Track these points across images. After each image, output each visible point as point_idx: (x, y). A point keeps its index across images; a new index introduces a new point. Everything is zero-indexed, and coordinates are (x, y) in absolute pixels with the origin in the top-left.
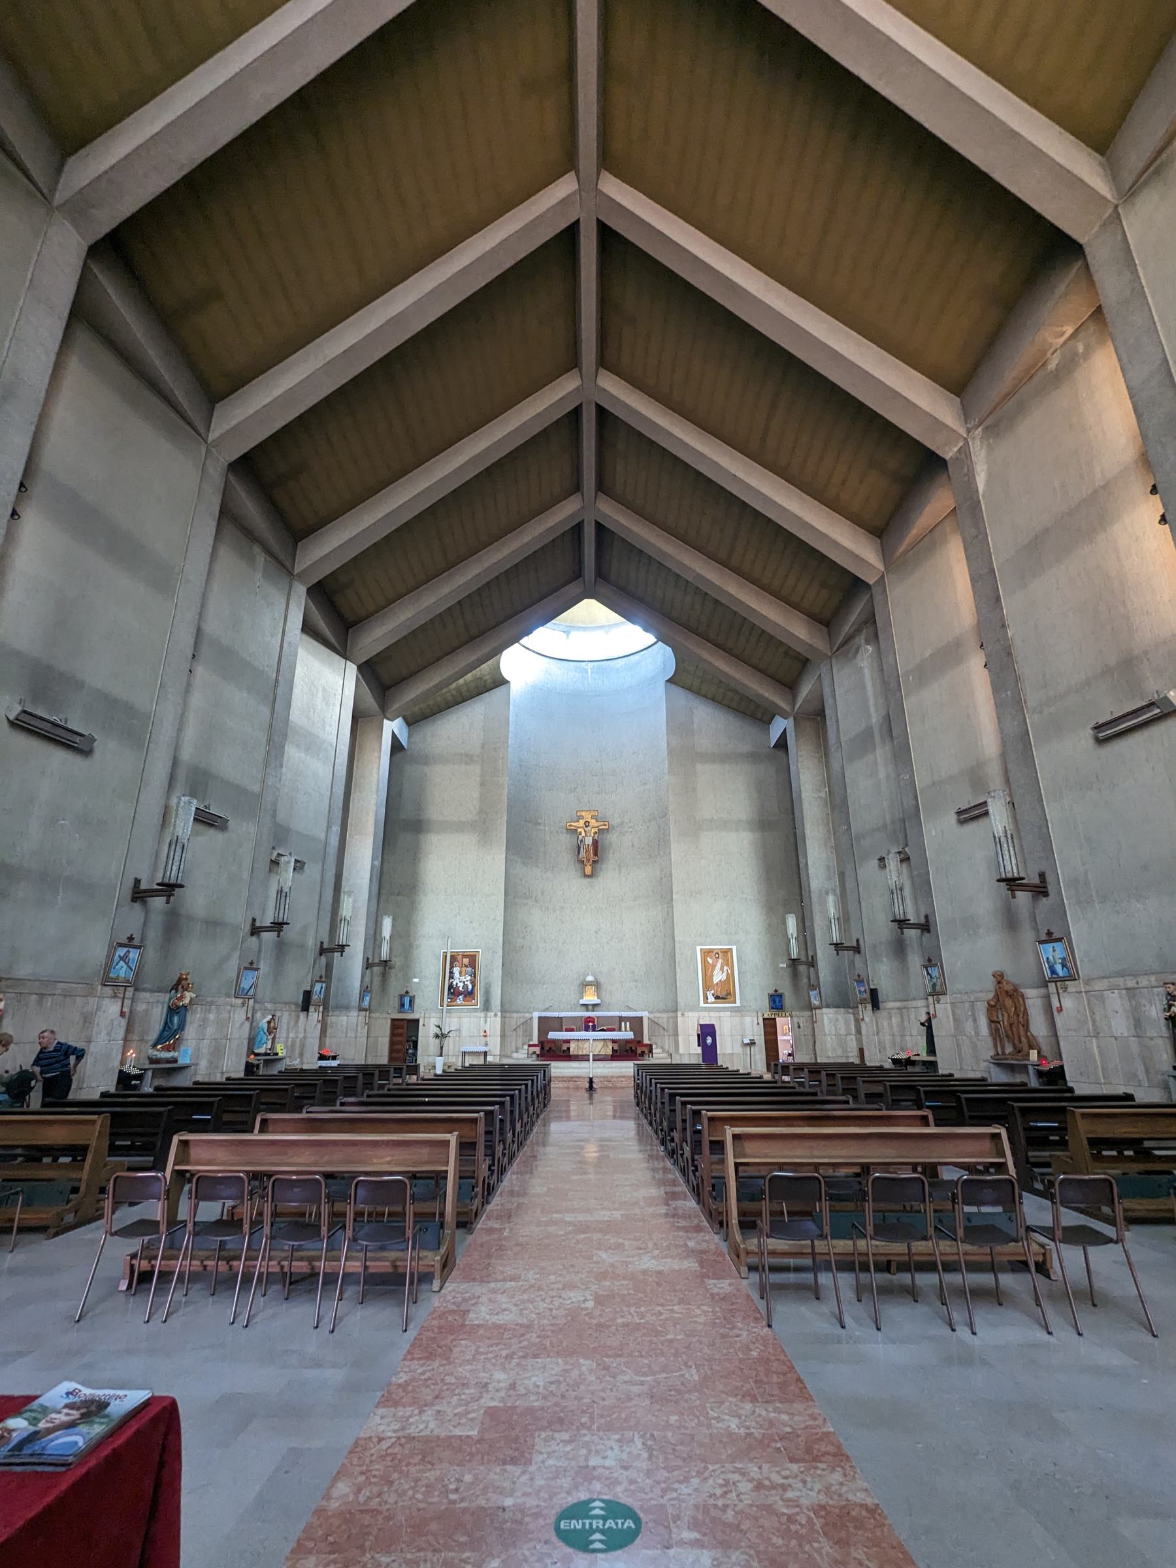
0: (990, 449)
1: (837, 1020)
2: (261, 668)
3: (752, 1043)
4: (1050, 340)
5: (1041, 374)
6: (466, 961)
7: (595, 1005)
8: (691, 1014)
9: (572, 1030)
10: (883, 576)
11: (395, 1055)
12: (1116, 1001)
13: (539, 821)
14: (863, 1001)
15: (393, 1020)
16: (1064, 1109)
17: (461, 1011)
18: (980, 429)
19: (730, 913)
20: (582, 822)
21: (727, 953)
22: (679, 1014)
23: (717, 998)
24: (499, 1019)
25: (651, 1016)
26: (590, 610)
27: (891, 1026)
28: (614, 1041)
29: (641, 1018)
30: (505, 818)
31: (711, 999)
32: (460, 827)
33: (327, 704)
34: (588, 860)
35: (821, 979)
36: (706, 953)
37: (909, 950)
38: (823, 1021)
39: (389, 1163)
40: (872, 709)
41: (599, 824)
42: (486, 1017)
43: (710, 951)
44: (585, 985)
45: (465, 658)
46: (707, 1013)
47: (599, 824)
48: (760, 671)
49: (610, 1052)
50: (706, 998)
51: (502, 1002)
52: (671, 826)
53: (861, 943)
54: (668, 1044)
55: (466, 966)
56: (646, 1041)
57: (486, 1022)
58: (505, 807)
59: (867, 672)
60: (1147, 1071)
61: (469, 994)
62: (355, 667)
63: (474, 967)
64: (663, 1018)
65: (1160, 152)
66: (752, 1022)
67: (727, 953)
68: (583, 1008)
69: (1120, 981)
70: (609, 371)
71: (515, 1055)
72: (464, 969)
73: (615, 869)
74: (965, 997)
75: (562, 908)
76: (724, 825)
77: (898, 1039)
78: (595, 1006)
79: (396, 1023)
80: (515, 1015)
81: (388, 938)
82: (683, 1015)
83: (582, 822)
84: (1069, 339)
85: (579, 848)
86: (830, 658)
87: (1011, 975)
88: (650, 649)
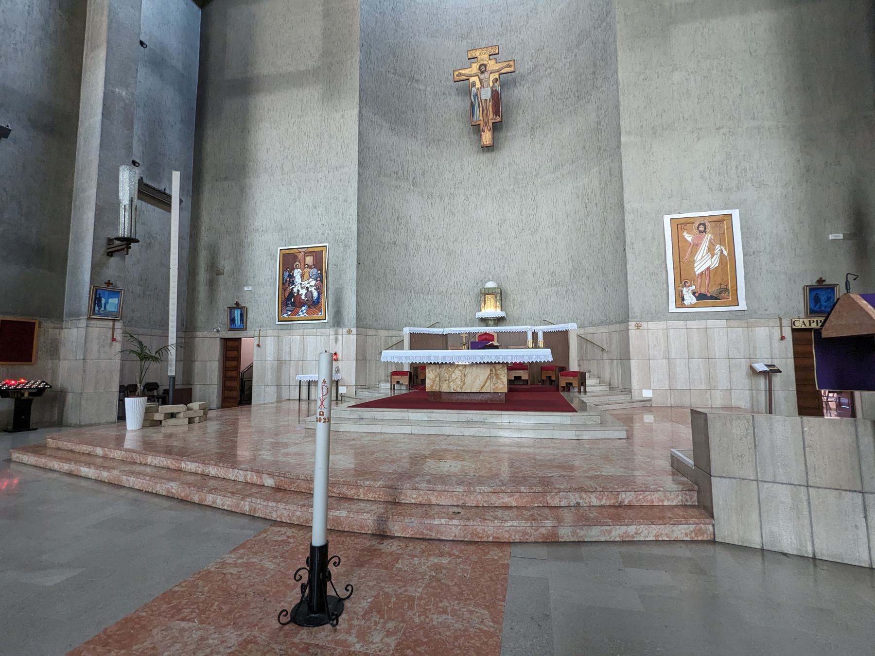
3: (771, 372)
6: (309, 260)
8: (652, 325)
11: (228, 383)
13: (417, 77)
17: (305, 327)
19: (728, 156)
20: (475, 67)
22: (632, 325)
23: (701, 297)
24: (353, 337)
25: (581, 332)
28: (512, 367)
29: (567, 332)
31: (690, 299)
32: (297, 79)
36: (679, 226)
41: (499, 66)
42: (336, 334)
44: (485, 293)
46: (681, 323)
49: (502, 386)
51: (358, 313)
54: (610, 370)
55: (310, 267)
56: (574, 367)
57: (336, 340)
61: (314, 304)
63: (320, 269)
64: (601, 334)
66: (771, 338)
72: (307, 270)
75: (453, 195)
78: (499, 321)
79: (229, 343)
80: (383, 333)
82: (638, 327)
85: (473, 106)
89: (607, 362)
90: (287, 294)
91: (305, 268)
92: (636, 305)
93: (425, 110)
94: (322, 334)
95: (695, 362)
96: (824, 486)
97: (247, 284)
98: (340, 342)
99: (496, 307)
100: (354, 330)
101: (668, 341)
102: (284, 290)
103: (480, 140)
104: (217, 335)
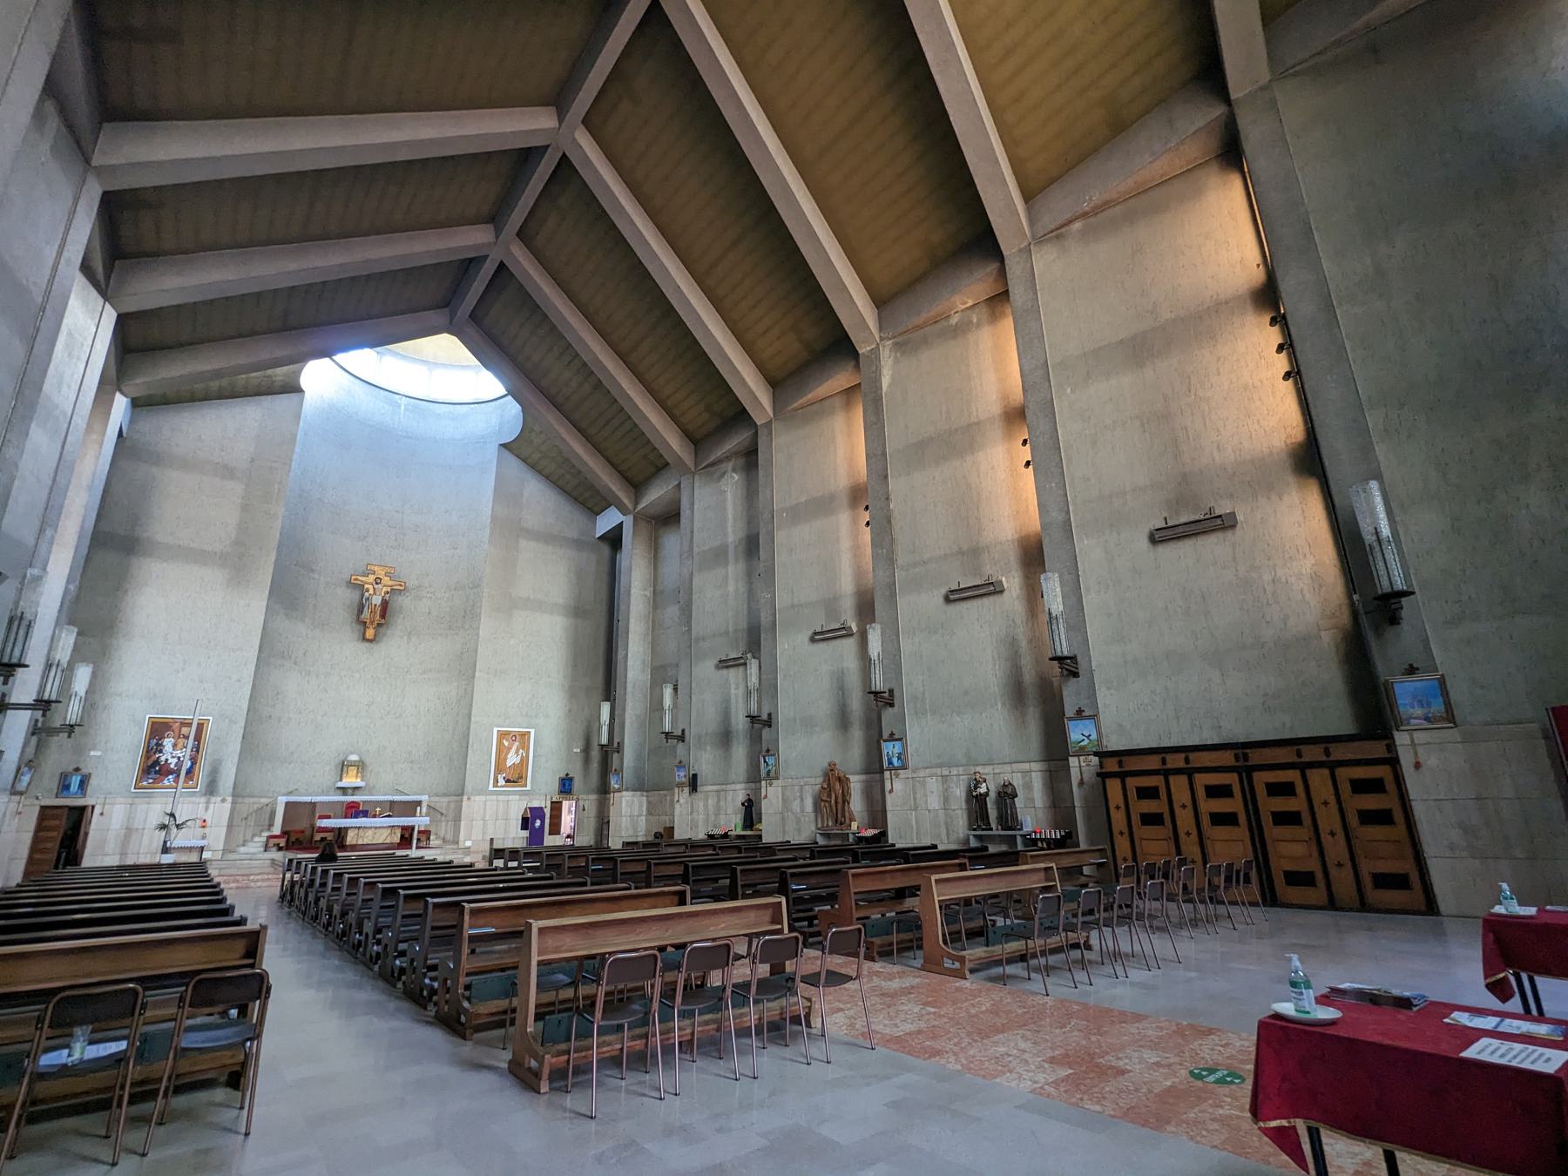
0: (896, 361)
1: (633, 802)
2: (24, 282)
4: (958, 303)
5: (944, 323)
7: (356, 789)
8: (477, 798)
9: (329, 817)
10: (771, 421)
12: (934, 785)
14: (680, 785)
15: (43, 808)
16: (838, 871)
18: (890, 342)
20: (371, 578)
21: (524, 736)
22: (465, 798)
23: (508, 781)
24: (228, 805)
26: (446, 346)
27: (706, 806)
30: (273, 559)
31: (501, 782)
32: (201, 557)
33: (70, 355)
34: (372, 623)
35: (625, 765)
36: (502, 735)
37: (735, 743)
38: (621, 804)
39: (723, 929)
40: (730, 530)
41: (393, 583)
42: (208, 803)
43: (507, 733)
44: (343, 767)
45: (265, 350)
46: (494, 797)
47: (393, 583)
48: (612, 464)
50: (496, 781)
51: (235, 783)
52: (484, 600)
53: (687, 733)
57: (207, 809)
58: (275, 544)
59: (729, 496)
60: (948, 834)
62: (115, 315)
64: (442, 803)
65: (1062, 226)
67: (524, 736)
68: (340, 792)
69: (938, 771)
70: (587, 128)
71: (242, 849)
73: (401, 637)
74: (795, 782)
76: (538, 606)
77: (712, 818)
79: (48, 812)
80: (248, 800)
81: (82, 693)
82: (469, 799)
83: (371, 578)
84: (967, 308)
85: (363, 607)
86: (694, 474)
87: (841, 768)
88: (483, 405)
89: (444, 824)
90: (150, 763)
91: (179, 737)
92: (469, 787)
93: (316, 596)
94: (190, 802)
95: (499, 822)
96: (76, 410)
97: (94, 748)
98: (211, 810)
99: (357, 777)
100: (230, 799)
101: (485, 809)
102: (148, 758)
103: (364, 634)
104: (37, 802)
